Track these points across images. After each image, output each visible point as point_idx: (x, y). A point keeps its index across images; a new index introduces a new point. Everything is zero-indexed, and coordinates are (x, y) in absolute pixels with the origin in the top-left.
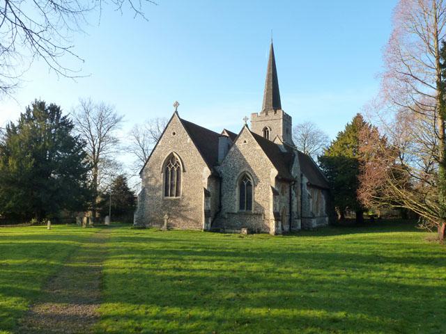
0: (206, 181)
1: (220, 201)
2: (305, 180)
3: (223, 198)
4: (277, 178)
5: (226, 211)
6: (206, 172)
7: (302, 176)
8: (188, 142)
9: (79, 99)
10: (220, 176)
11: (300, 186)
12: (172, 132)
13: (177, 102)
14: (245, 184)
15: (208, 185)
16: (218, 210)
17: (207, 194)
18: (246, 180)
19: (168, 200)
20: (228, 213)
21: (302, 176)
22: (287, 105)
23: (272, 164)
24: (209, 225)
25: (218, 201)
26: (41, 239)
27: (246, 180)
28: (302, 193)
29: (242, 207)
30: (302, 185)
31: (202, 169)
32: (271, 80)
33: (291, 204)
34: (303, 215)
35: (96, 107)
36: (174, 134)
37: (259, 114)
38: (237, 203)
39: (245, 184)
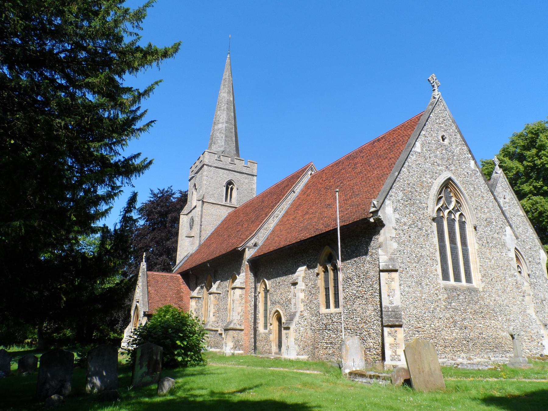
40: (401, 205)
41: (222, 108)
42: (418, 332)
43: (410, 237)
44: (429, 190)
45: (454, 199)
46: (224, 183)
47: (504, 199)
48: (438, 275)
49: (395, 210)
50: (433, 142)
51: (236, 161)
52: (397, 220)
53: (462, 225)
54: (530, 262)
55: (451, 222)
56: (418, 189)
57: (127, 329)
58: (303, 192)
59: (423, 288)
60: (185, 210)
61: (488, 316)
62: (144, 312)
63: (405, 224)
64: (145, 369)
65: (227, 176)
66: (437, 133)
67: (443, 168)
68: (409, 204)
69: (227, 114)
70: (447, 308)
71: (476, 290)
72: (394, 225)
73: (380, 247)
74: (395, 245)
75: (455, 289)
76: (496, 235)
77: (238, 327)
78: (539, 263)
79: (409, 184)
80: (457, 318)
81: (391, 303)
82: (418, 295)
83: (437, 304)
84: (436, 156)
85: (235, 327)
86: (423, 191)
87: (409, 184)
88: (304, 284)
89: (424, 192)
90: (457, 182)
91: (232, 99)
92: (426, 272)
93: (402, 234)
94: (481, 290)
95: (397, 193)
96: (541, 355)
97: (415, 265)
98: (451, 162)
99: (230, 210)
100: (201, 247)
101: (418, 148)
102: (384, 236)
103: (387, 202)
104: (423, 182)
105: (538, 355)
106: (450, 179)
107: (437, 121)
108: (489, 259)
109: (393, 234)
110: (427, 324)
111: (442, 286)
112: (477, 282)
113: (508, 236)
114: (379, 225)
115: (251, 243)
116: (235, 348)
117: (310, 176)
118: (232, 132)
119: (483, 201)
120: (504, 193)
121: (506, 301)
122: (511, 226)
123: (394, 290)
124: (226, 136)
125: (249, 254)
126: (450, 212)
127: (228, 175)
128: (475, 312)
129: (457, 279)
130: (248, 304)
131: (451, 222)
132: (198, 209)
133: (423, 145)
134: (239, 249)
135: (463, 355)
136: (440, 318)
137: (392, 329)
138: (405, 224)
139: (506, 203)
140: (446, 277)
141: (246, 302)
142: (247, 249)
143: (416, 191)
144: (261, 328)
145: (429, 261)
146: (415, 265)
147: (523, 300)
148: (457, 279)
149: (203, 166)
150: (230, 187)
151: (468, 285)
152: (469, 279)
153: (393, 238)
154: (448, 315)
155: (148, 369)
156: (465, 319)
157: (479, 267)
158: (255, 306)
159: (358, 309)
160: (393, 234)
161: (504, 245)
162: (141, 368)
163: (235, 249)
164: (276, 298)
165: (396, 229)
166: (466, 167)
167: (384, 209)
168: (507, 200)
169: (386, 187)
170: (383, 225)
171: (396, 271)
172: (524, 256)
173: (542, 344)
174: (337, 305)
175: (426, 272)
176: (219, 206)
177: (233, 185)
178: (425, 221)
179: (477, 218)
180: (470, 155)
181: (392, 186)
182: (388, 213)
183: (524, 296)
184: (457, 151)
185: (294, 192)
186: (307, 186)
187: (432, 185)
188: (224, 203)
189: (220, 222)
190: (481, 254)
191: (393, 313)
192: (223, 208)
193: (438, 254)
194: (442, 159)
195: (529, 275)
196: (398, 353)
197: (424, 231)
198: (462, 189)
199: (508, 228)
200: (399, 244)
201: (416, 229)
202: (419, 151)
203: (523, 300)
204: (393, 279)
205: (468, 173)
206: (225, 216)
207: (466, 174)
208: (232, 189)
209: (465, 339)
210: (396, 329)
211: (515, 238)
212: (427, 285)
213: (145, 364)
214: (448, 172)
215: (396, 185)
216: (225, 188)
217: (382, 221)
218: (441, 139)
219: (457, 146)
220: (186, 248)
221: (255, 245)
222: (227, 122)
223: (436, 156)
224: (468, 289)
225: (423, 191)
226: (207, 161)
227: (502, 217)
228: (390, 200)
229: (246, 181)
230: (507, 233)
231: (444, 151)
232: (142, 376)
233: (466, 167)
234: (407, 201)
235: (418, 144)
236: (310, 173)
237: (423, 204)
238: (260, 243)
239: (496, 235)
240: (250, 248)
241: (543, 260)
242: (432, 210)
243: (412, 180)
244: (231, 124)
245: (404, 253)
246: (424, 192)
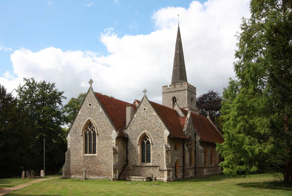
0: (114, 141)
1: (127, 155)
2: (198, 138)
3: (129, 154)
4: (169, 137)
5: (132, 164)
6: (114, 134)
7: (195, 135)
8: (100, 111)
9: (25, 79)
10: (126, 137)
11: (194, 143)
12: (89, 104)
13: (91, 80)
14: (145, 142)
15: (116, 145)
16: (125, 163)
17: (115, 152)
18: (146, 140)
19: (87, 156)
20: (133, 166)
21: (195, 135)
22: (191, 79)
23: (165, 127)
24: (117, 175)
25: (125, 156)
26: (147, 151)
27: (146, 140)
28: (195, 148)
29: (143, 161)
30: (195, 142)
31: (111, 133)
32: (178, 57)
33: (184, 157)
34: (197, 166)
35: (38, 86)
36: (90, 105)
37: (168, 87)
38: (139, 158)
39: (145, 142)
46: (171, 99)
52: (71, 139)
80: (86, 165)
92: (78, 152)
121: (107, 159)
128: (93, 163)
165: (70, 142)
175: (78, 152)
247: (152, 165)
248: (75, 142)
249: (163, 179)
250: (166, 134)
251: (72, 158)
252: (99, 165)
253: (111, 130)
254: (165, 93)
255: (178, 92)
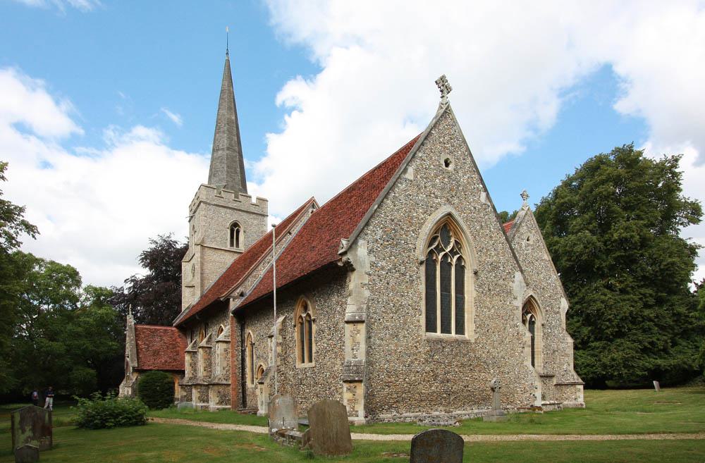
40: (379, 245)
41: (222, 130)
42: (389, 387)
43: (388, 284)
44: (420, 228)
45: (453, 240)
46: (228, 225)
47: (528, 240)
48: (420, 326)
49: (370, 252)
50: (432, 167)
51: (241, 198)
52: (373, 265)
53: (460, 270)
54: (547, 311)
55: (446, 266)
56: (405, 227)
57: (122, 384)
58: (300, 234)
59: (399, 340)
60: (186, 258)
61: (477, 369)
62: (133, 368)
63: (383, 268)
64: (29, 433)
65: (231, 217)
66: (440, 156)
67: (443, 200)
68: (390, 244)
69: (229, 138)
70: (427, 361)
71: (466, 342)
72: (368, 269)
73: (350, 295)
74: (367, 293)
75: (440, 341)
76: (501, 282)
77: (224, 382)
78: (558, 312)
79: (393, 221)
80: (439, 371)
81: (355, 357)
82: (393, 348)
83: (415, 357)
84: (434, 186)
85: (220, 382)
86: (411, 229)
87: (393, 221)
88: (281, 337)
89: (413, 231)
90: (459, 219)
91: (233, 118)
92: (405, 323)
93: (377, 281)
94: (473, 341)
95: (376, 232)
96: (532, 406)
97: (391, 315)
98: (454, 194)
99: (236, 256)
100: (203, 297)
101: (410, 175)
102: (354, 281)
103: (361, 242)
104: (412, 218)
105: (529, 406)
106: (450, 214)
107: (441, 140)
108: (488, 308)
109: (366, 280)
110: (400, 379)
111: (424, 338)
112: (469, 334)
113: (517, 283)
114: (349, 268)
115: (236, 293)
116: (220, 403)
117: (310, 215)
118: (235, 162)
119: (491, 243)
120: (529, 234)
121: (502, 353)
122: (522, 271)
123: (359, 343)
124: (228, 167)
125: (234, 304)
126: (445, 256)
127: (232, 215)
128: (463, 365)
129: (446, 329)
130: (235, 359)
131: (446, 266)
132: (198, 255)
133: (417, 171)
134: (222, 299)
135: (441, 408)
136: (418, 372)
137: (352, 385)
138: (383, 268)
139: (529, 245)
140: (431, 327)
141: (232, 357)
142: (231, 300)
143: (403, 229)
144: (249, 385)
145: (411, 311)
146: (391, 315)
147: (522, 352)
148: (446, 329)
149: (200, 203)
150: (236, 229)
151: (458, 336)
152: (460, 330)
153: (366, 284)
154: (428, 369)
155: (34, 433)
156: (449, 372)
157: (473, 318)
158: (243, 360)
159: (329, 363)
160: (366, 280)
161: (509, 293)
162: (23, 431)
163: (216, 300)
164: (260, 352)
165: (370, 275)
166: (474, 200)
167: (356, 249)
168: (531, 242)
169: (361, 224)
170: (353, 270)
171: (363, 322)
172: (540, 305)
173: (534, 395)
174: (310, 361)
175: (405, 323)
176: (223, 252)
177: (239, 227)
178: (411, 265)
179: (480, 262)
180: (481, 186)
181: (368, 221)
182: (362, 255)
183: (523, 348)
184: (464, 180)
185: (290, 234)
186: (305, 227)
187: (424, 222)
188: (228, 247)
189: (224, 271)
190: (479, 303)
191: (355, 368)
192: (227, 254)
193: (423, 303)
194: (443, 189)
195: (543, 325)
196: (356, 409)
197: (408, 277)
198: (465, 228)
199: (518, 275)
200: (372, 291)
201: (397, 274)
202: (411, 178)
203: (522, 352)
204: (358, 332)
205: (475, 208)
206: (231, 264)
207: (472, 208)
208: (238, 232)
209: (445, 393)
210: (356, 384)
211: (525, 285)
212: (405, 337)
213: (28, 428)
214: (448, 206)
215: (375, 221)
216: (229, 231)
217: (352, 265)
218: (444, 164)
219: (465, 174)
220: (190, 298)
221: (242, 295)
222: (228, 149)
223: (434, 186)
224: (457, 340)
225: (411, 229)
226: (204, 198)
227: (512, 260)
228: (364, 239)
229: (255, 222)
230: (516, 279)
231: (446, 180)
232: (26, 441)
233: (474, 200)
234: (388, 241)
235: (411, 170)
236: (310, 210)
237: (410, 245)
238: (248, 292)
239: (501, 282)
240: (234, 298)
241: (564, 309)
242: (420, 253)
243: (397, 215)
244: (234, 151)
245: (378, 302)
246: (413, 231)
247: (542, 372)
248: (392, 283)
249: (203, 404)
250: (564, 309)
251: (378, 342)
252: (479, 371)
253: (511, 269)
254: (209, 204)
255: (245, 213)
